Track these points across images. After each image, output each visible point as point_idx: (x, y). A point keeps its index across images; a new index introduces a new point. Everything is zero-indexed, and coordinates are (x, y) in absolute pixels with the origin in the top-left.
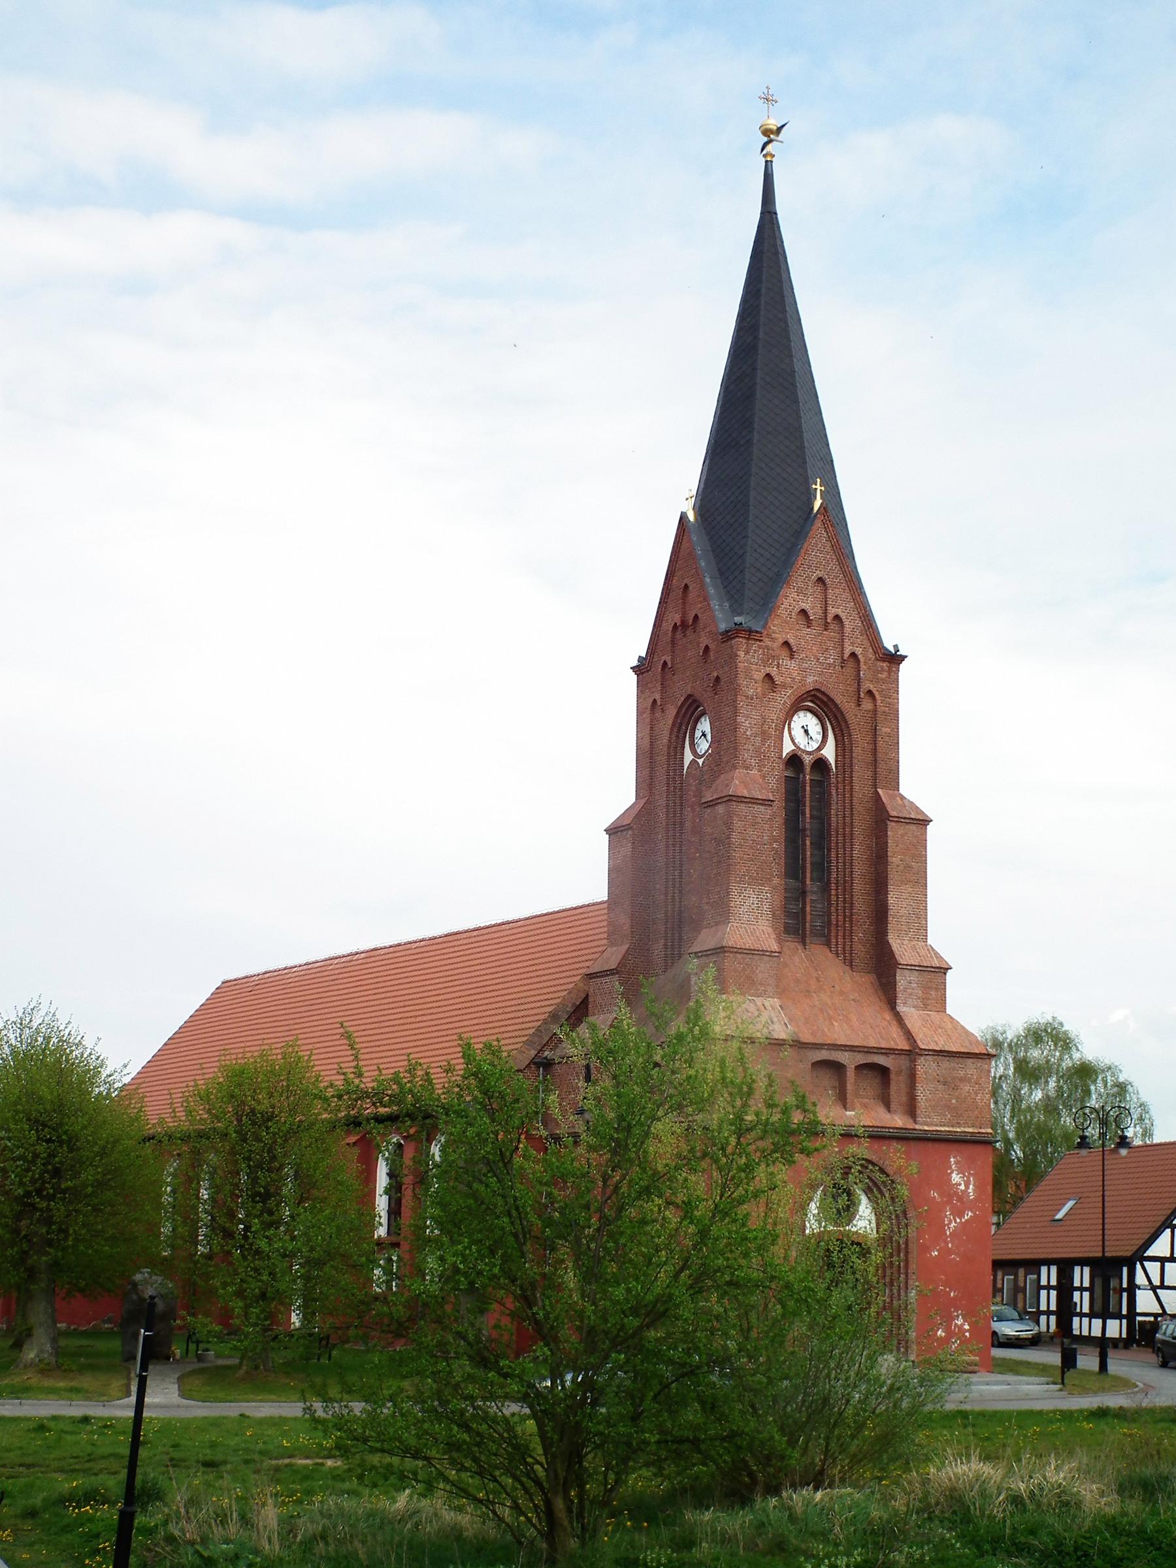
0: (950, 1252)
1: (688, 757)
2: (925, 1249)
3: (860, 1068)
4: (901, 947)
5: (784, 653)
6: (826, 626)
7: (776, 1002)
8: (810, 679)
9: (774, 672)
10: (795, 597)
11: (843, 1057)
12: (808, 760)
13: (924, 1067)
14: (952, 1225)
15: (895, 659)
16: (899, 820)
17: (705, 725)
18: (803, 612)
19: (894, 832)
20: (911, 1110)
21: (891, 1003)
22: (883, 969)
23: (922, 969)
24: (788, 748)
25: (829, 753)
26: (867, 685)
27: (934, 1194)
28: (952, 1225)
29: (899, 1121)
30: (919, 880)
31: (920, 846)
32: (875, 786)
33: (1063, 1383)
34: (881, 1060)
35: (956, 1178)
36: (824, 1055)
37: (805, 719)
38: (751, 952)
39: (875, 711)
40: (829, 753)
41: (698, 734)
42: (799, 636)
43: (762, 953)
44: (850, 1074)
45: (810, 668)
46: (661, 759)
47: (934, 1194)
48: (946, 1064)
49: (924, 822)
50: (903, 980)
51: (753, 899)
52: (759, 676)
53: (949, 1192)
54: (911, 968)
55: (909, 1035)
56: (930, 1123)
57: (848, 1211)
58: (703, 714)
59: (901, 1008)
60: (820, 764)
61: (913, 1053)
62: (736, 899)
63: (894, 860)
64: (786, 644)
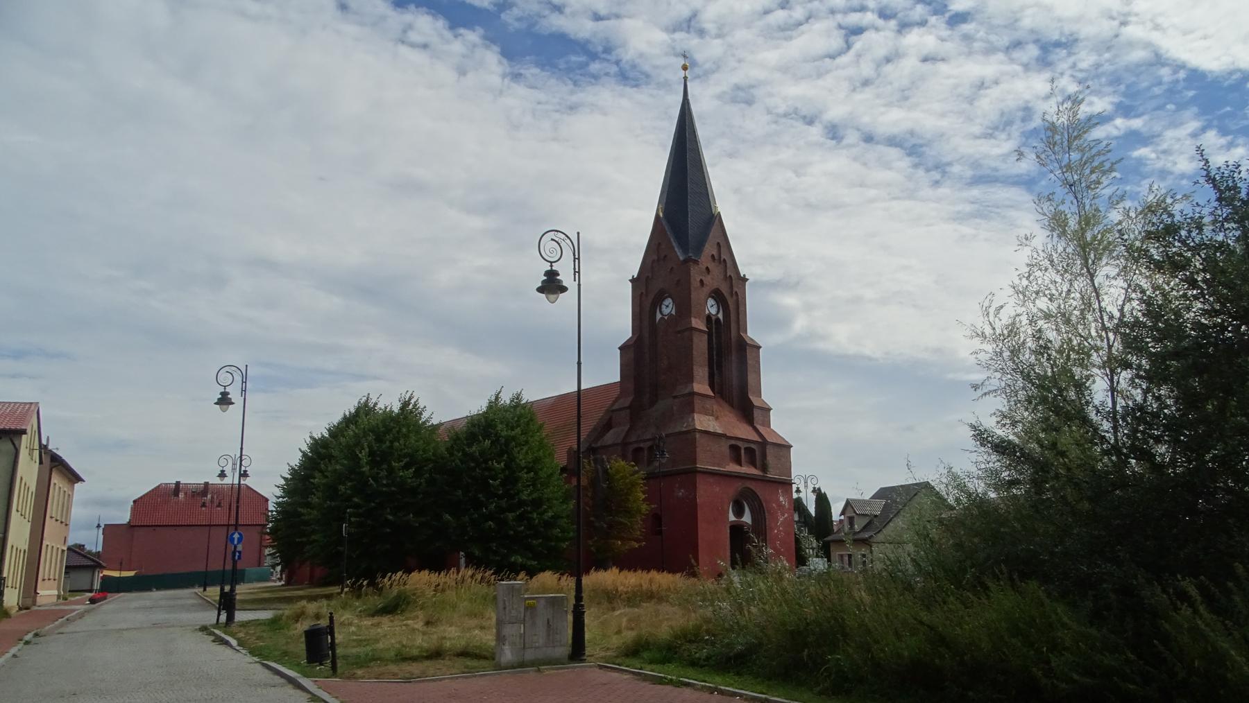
1: (659, 316)
11: (740, 444)
20: (764, 468)
25: (720, 316)
34: (753, 446)
36: (733, 442)
37: (711, 302)
42: (711, 266)
45: (714, 280)
50: (756, 413)
53: (780, 505)
56: (770, 475)
57: (739, 512)
60: (718, 319)
62: (695, 373)
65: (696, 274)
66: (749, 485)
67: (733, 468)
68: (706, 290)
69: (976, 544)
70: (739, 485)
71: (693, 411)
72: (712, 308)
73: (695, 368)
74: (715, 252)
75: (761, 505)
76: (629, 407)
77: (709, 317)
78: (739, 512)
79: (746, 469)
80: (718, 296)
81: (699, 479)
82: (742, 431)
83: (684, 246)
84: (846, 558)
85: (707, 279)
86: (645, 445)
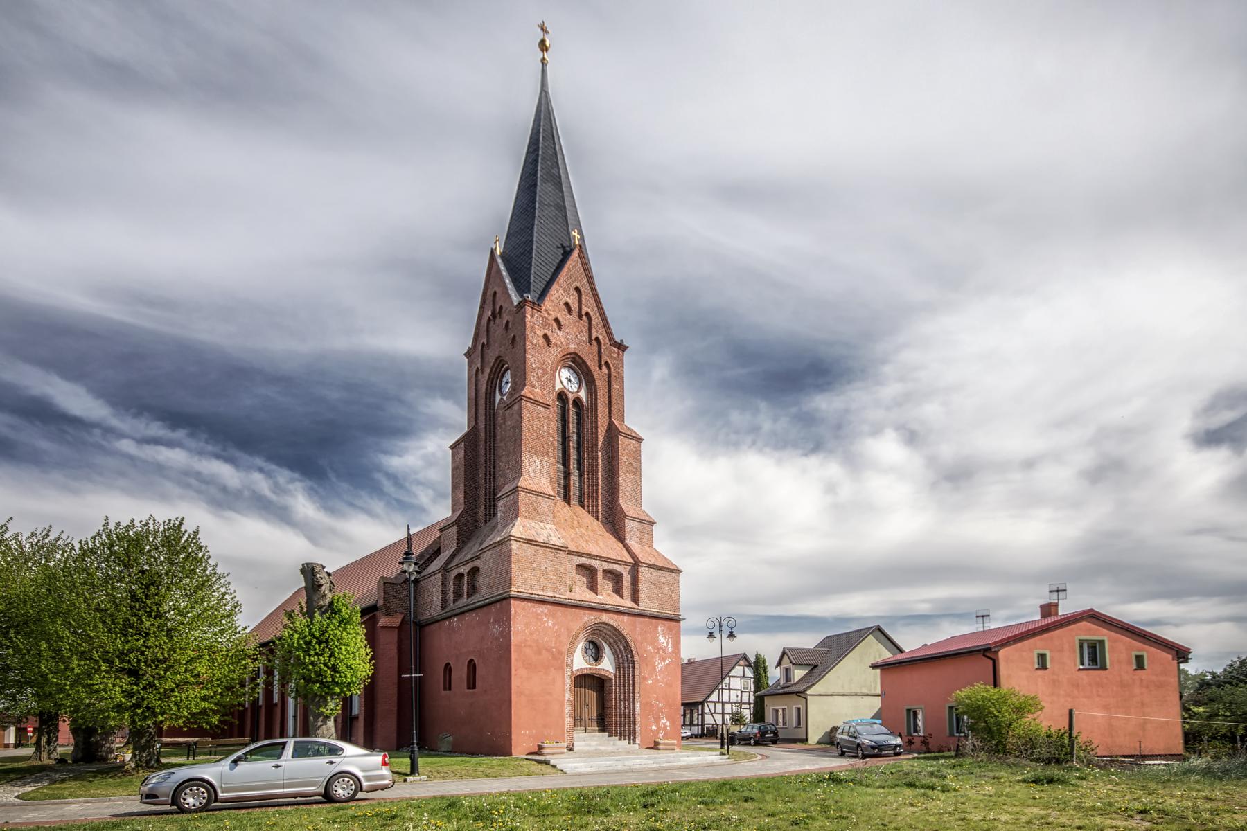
0: (658, 681)
1: (498, 397)
2: (645, 679)
3: (605, 571)
4: (625, 504)
5: (555, 325)
6: (580, 316)
7: (553, 527)
8: (572, 346)
9: (549, 334)
10: (559, 293)
12: (571, 397)
13: (643, 573)
14: (660, 666)
15: (621, 347)
16: (627, 436)
17: (508, 377)
18: (567, 304)
19: (623, 442)
20: (635, 599)
21: (621, 539)
22: (614, 522)
23: (640, 520)
24: (558, 387)
25: (583, 395)
26: (605, 358)
27: (650, 648)
28: (660, 666)
29: (628, 603)
30: (637, 472)
31: (636, 455)
32: (610, 417)
33: (702, 703)
34: (617, 568)
35: (661, 639)
36: (583, 560)
37: (565, 373)
38: (537, 493)
39: (609, 375)
40: (583, 395)
41: (505, 380)
43: (544, 495)
44: (600, 574)
45: (571, 337)
46: (482, 402)
47: (650, 648)
48: (656, 573)
49: (639, 440)
50: (630, 526)
51: (537, 463)
52: (540, 333)
53: (659, 649)
54: (633, 519)
55: (633, 555)
56: (645, 605)
57: (597, 657)
58: (507, 369)
59: (627, 541)
60: (577, 402)
61: (635, 565)
62: (525, 462)
63: (623, 458)
64: (556, 320)
65: (530, 317)
66: (605, 617)
67: (581, 593)
68: (554, 354)
69: (184, 428)
70: (589, 618)
71: (517, 516)
72: (566, 380)
73: (525, 455)
74: (573, 300)
75: (627, 647)
76: (457, 522)
77: (562, 396)
78: (596, 653)
79: (606, 595)
80: (576, 363)
81: (879, 692)
82: (600, 543)
83: (522, 285)
84: (780, 712)
85: (557, 336)
86: (464, 570)
